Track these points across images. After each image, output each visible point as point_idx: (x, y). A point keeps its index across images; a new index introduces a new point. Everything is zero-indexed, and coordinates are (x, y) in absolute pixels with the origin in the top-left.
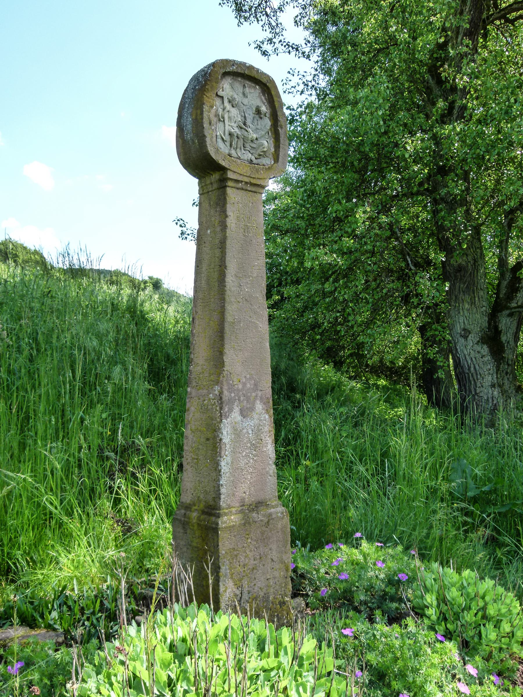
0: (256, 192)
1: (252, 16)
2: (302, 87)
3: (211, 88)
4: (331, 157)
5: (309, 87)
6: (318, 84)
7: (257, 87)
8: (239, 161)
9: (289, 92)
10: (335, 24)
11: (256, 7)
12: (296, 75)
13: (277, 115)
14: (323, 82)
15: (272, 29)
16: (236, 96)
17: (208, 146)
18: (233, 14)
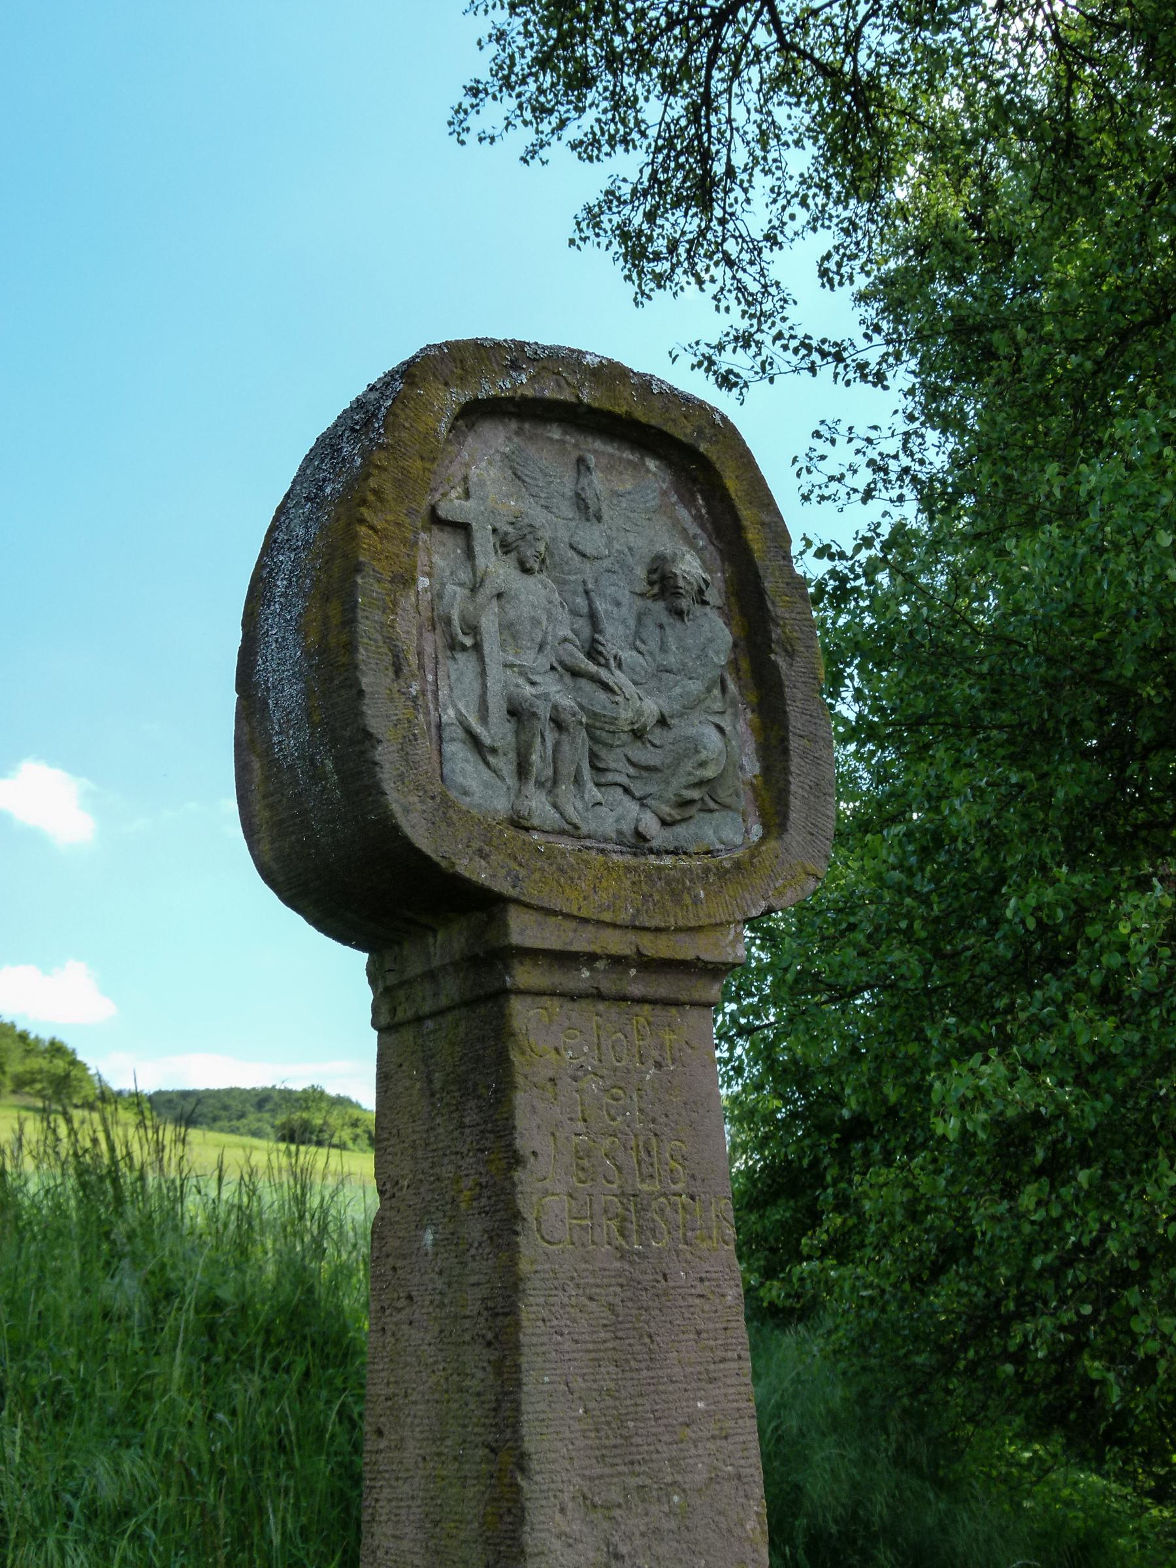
0: (677, 1004)
1: (679, 270)
2: (865, 476)
3: (399, 483)
4: (994, 706)
5: (893, 476)
6: (922, 462)
7: (651, 464)
8: (565, 844)
9: (823, 498)
10: (956, 277)
11: (690, 242)
12: (841, 440)
13: (761, 593)
14: (937, 452)
15: (749, 304)
16: (539, 517)
17: (388, 786)
18: (618, 270)
